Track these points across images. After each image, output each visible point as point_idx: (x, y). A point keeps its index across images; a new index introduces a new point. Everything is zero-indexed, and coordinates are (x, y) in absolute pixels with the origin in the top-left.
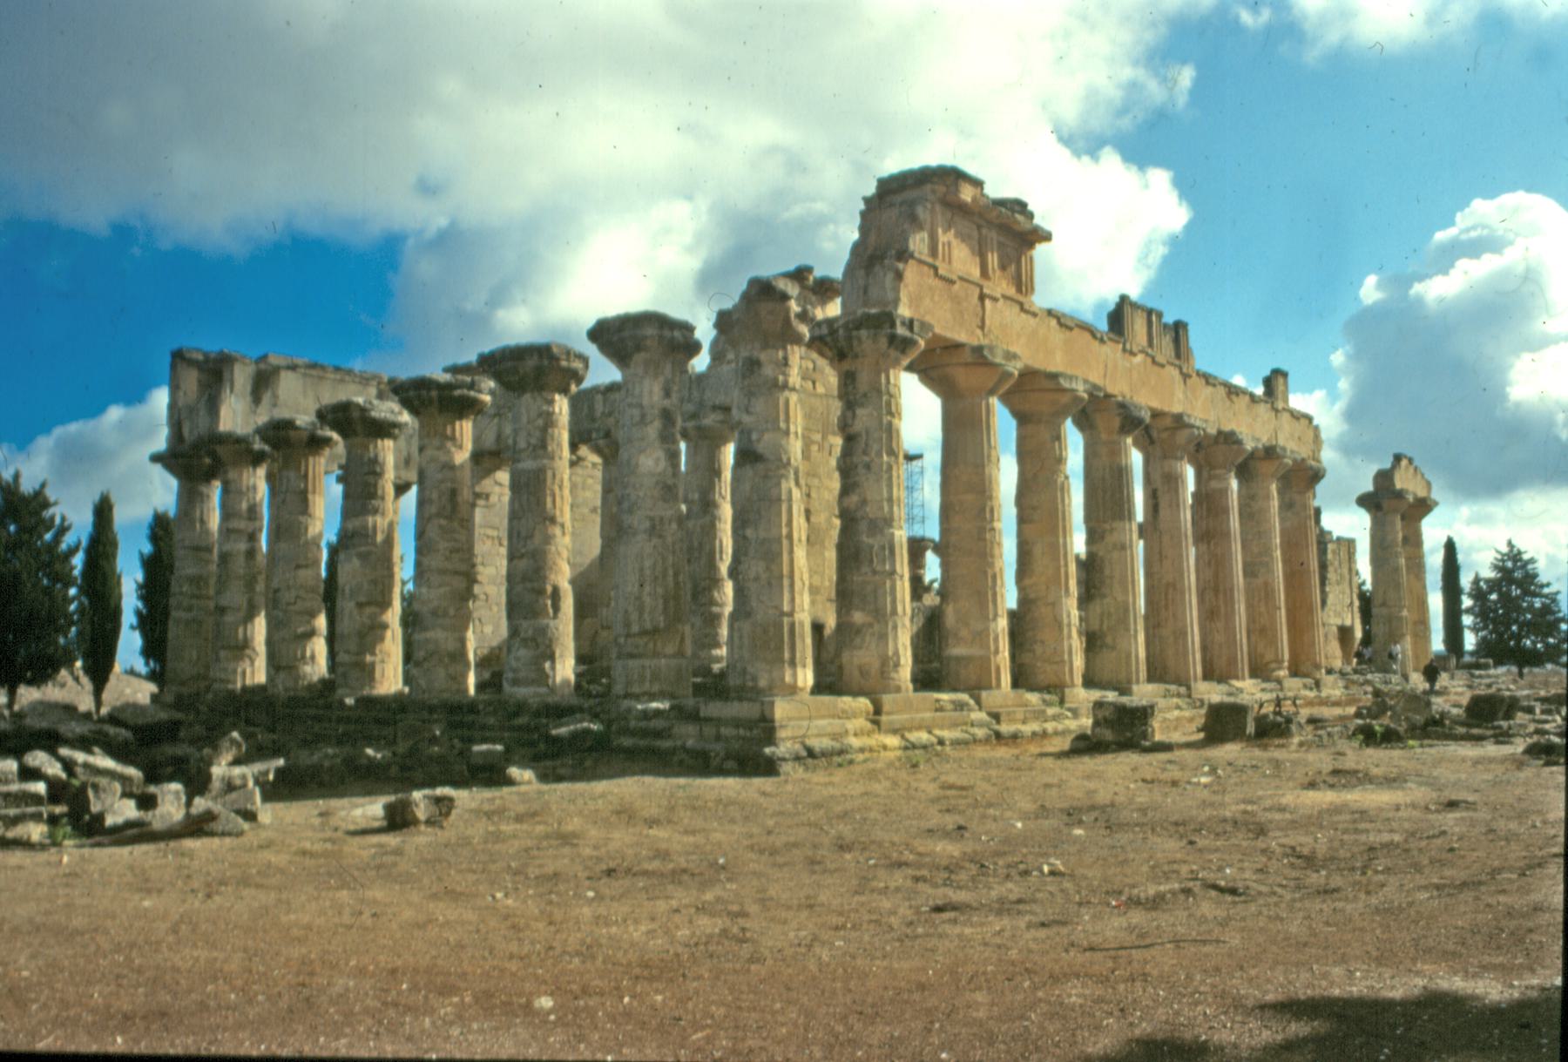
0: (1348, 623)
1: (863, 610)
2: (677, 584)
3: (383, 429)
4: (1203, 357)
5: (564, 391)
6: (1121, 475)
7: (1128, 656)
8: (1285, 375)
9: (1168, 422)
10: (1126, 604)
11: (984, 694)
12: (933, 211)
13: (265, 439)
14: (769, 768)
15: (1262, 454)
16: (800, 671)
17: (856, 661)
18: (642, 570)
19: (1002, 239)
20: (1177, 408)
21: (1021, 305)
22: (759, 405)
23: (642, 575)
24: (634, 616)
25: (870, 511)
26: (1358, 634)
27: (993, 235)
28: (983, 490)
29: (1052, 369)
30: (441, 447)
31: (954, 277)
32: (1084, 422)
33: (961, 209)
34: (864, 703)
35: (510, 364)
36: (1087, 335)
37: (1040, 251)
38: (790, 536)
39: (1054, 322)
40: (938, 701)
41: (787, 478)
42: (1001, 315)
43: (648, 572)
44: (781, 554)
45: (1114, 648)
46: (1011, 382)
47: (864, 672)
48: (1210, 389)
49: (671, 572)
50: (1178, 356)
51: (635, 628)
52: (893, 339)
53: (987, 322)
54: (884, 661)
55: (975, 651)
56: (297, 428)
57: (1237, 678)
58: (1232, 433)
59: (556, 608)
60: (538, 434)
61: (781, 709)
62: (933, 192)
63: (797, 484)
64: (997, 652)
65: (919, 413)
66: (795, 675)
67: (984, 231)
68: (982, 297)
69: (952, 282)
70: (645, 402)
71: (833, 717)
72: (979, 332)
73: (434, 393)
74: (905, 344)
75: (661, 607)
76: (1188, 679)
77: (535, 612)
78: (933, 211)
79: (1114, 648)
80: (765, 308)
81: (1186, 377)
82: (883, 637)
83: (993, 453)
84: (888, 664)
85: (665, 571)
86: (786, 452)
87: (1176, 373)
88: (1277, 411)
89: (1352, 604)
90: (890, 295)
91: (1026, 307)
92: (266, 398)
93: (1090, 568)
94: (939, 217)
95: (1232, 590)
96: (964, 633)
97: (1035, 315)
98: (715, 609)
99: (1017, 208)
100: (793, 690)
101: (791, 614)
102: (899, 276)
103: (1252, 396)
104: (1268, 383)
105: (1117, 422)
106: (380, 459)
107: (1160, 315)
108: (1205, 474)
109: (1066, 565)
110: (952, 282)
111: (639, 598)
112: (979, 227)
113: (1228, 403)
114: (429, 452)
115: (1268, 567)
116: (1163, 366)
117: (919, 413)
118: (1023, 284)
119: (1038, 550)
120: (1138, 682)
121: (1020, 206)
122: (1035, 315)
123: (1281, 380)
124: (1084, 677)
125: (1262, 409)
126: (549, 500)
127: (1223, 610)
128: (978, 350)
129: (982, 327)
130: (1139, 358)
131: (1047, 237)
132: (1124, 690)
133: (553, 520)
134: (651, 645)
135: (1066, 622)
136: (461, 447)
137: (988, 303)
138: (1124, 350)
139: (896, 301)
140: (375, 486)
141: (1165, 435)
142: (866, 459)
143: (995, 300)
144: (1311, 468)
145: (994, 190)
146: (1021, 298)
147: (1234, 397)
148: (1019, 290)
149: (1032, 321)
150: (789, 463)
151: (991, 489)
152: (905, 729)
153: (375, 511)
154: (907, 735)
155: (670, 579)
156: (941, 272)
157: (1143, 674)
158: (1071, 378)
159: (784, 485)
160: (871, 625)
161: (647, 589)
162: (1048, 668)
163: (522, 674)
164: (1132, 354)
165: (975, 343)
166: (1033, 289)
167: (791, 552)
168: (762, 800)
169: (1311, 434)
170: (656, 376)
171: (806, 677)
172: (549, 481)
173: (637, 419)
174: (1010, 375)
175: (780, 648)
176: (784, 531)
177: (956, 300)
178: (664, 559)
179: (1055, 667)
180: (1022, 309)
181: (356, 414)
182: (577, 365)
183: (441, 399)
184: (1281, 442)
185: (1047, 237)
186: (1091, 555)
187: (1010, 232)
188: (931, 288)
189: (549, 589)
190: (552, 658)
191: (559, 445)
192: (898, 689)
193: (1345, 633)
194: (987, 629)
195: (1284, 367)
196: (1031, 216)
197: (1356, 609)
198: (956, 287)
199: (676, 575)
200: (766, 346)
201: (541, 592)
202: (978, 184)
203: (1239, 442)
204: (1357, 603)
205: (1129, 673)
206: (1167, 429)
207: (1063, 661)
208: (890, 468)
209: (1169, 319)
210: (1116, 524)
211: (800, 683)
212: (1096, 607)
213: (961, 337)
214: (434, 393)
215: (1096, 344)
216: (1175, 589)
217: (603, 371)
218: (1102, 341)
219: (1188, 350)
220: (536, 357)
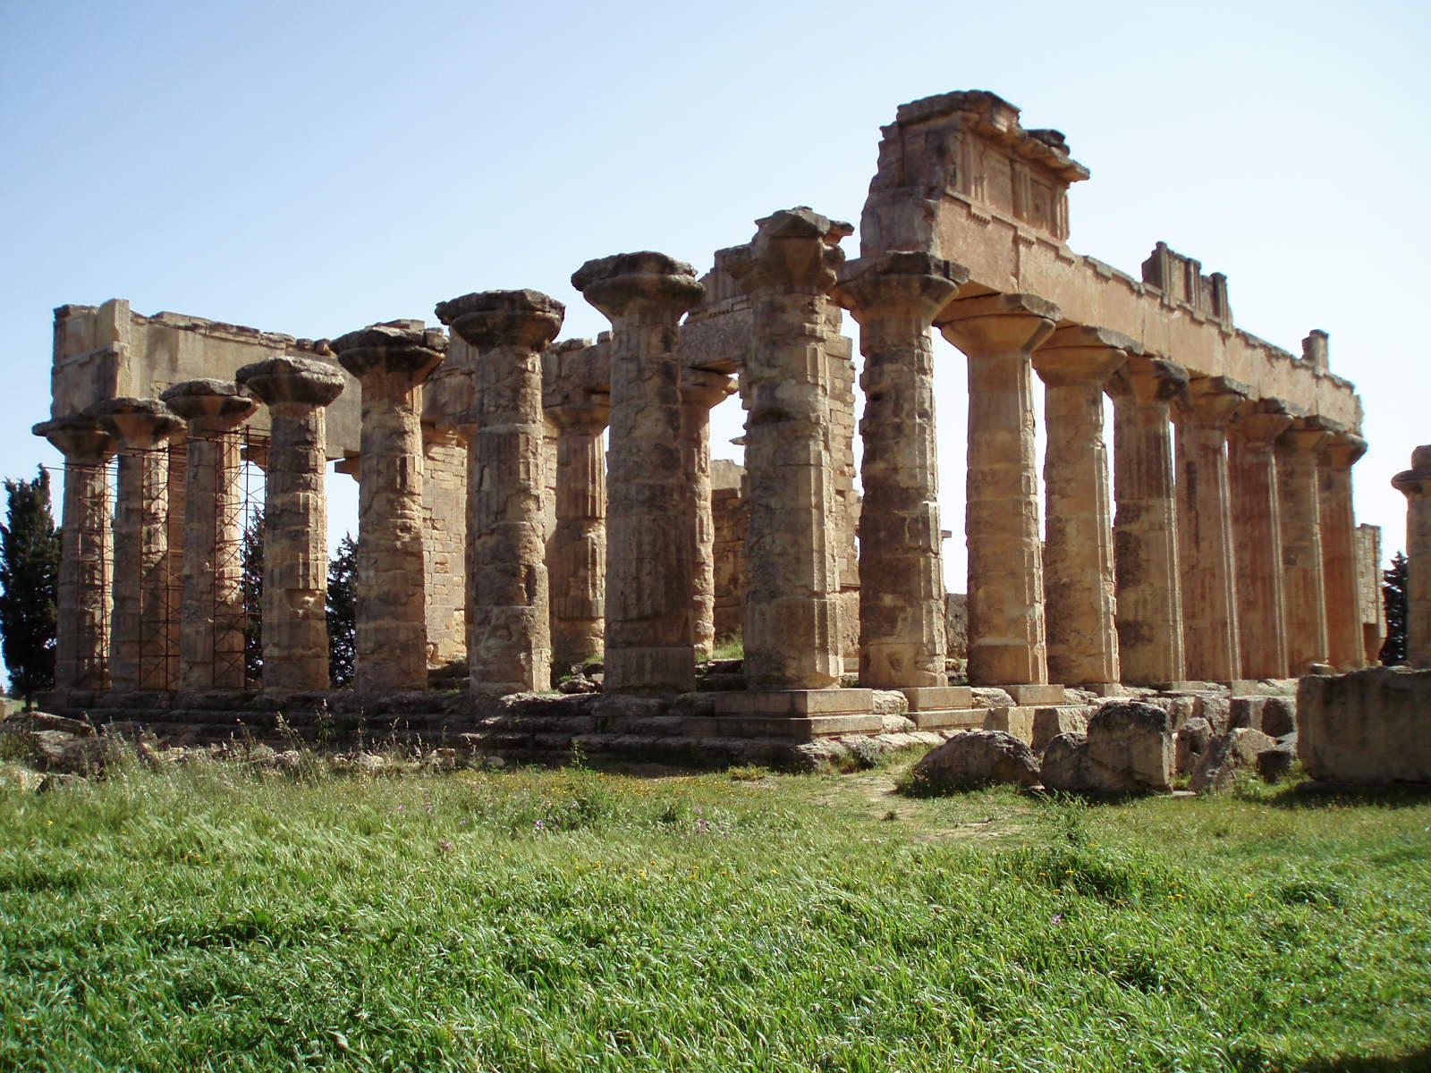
0: (1372, 620)
1: (893, 592)
2: (679, 560)
3: (325, 394)
4: (1245, 312)
5: (538, 348)
6: (1159, 441)
7: (1167, 649)
8: (1325, 336)
9: (1205, 387)
10: (1164, 588)
11: (1022, 689)
12: (963, 143)
13: (172, 407)
14: (804, 765)
15: (1301, 425)
16: (831, 657)
17: (886, 650)
18: (639, 545)
19: (1035, 176)
20: (1215, 372)
21: (1056, 249)
22: (782, 357)
23: (640, 552)
24: (632, 599)
25: (903, 480)
26: (1383, 633)
27: (1026, 171)
28: (1016, 455)
29: (1087, 322)
30: (390, 410)
31: (989, 218)
32: (1119, 388)
33: (993, 139)
34: (894, 696)
35: (475, 314)
36: (1124, 288)
37: (1075, 191)
38: (820, 506)
39: (1089, 272)
40: (975, 695)
41: (816, 440)
42: (1036, 263)
43: (646, 548)
44: (810, 525)
45: (1150, 640)
46: (1048, 335)
47: (894, 662)
48: (1249, 352)
49: (673, 549)
50: (1216, 311)
51: (633, 613)
52: (927, 285)
53: (1022, 270)
54: (918, 647)
55: (1011, 640)
56: (212, 393)
57: (1277, 677)
58: (1273, 401)
59: (532, 593)
60: (508, 393)
61: (815, 702)
62: (965, 120)
63: (827, 448)
64: (1034, 641)
65: (947, 371)
66: (827, 663)
67: (1018, 167)
68: (1017, 240)
69: (985, 222)
70: (643, 354)
71: (867, 712)
72: (1013, 279)
73: (382, 350)
74: (934, 290)
75: (662, 589)
76: (1227, 676)
77: (506, 598)
78: (963, 143)
79: (1150, 640)
80: (793, 246)
81: (1225, 336)
82: (917, 623)
83: (1029, 416)
84: (925, 653)
85: (667, 546)
86: (815, 411)
87: (1214, 331)
88: (1317, 377)
89: (1377, 601)
90: (920, 236)
91: (1062, 253)
92: (162, 356)
94: (971, 148)
95: (1271, 578)
96: (997, 619)
97: (1070, 262)
98: (697, 598)
99: (1053, 141)
100: (826, 680)
101: (821, 595)
102: (930, 214)
103: (1292, 359)
104: (1308, 344)
105: (1154, 385)
106: (312, 426)
107: (1198, 266)
108: (1240, 446)
109: (1104, 546)
110: (985, 222)
111: (637, 578)
112: (1012, 162)
113: (1268, 365)
114: (375, 416)
115: (1308, 552)
116: (1200, 323)
117: (947, 371)
118: (1059, 228)
119: (1071, 529)
120: (1177, 679)
121: (1056, 138)
122: (1070, 262)
123: (1321, 341)
124: (1189, 665)
125: (1304, 375)
126: (522, 468)
127: (1261, 601)
128: (1015, 299)
129: (1016, 275)
130: (1177, 314)
131: (1085, 175)
132: (1162, 689)
133: (526, 491)
134: (651, 632)
135: (1103, 609)
136: (411, 411)
137: (1022, 248)
138: (1162, 305)
139: (928, 243)
140: (307, 457)
141: (1202, 401)
142: (897, 420)
143: (1029, 243)
144: (1353, 442)
145: (1028, 122)
146: (1053, 241)
147: (1274, 360)
148: (1054, 234)
149: (1068, 269)
150: (817, 423)
151: (1027, 458)
152: (943, 727)
153: (307, 486)
154: (946, 733)
155: (673, 557)
156: (974, 210)
157: (1182, 671)
158: (1107, 332)
159: (812, 446)
160: (902, 609)
161: (647, 568)
162: (1086, 661)
163: (492, 667)
164: (1171, 310)
165: (1011, 292)
166: (1068, 233)
167: (821, 523)
169: (1351, 404)
170: (654, 325)
171: (837, 666)
172: (522, 448)
173: (633, 375)
174: (1050, 327)
175: (810, 633)
176: (813, 500)
177: (988, 242)
178: (665, 533)
179: (1091, 659)
180: (1059, 257)
181: (284, 376)
182: (554, 315)
183: (390, 356)
184: (1322, 413)
185: (1085, 175)
187: (1043, 167)
188: (963, 228)
189: (524, 571)
190: (528, 649)
191: (533, 407)
192: (933, 681)
193: (1370, 629)
194: (1023, 616)
195: (1325, 329)
196: (1066, 150)
197: (1381, 606)
198: (990, 227)
199: (679, 551)
200: (789, 291)
201: (515, 574)
202: (1014, 112)
203: (1281, 411)
204: (1382, 599)
205: (1167, 669)
206: (1205, 395)
207: (1101, 653)
208: (923, 430)
209: (1206, 271)
210: (1155, 502)
211: (832, 674)
212: (1131, 596)
213: (996, 286)
214: (382, 350)
215: (1134, 297)
216: (1213, 575)
217: (584, 323)
218: (1139, 294)
219: (1227, 309)
220: (507, 306)
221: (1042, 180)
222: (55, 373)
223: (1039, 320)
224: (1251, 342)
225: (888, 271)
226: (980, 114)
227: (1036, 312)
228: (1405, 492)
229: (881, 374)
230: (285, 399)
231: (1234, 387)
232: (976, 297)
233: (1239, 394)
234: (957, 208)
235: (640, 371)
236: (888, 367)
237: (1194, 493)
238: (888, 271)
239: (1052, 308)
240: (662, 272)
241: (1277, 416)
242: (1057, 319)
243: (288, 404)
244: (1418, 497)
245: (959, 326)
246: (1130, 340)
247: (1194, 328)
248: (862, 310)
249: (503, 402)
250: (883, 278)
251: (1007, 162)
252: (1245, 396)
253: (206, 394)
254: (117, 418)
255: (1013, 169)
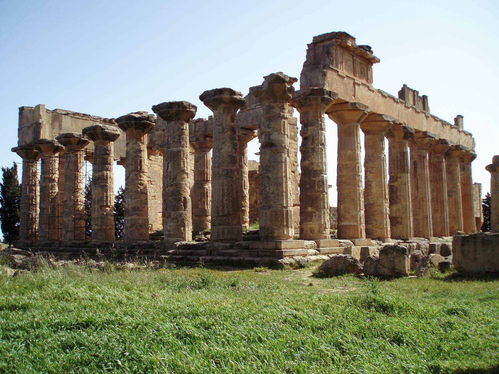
0: (479, 216)
1: (311, 206)
2: (237, 195)
3: (113, 137)
4: (434, 109)
5: (188, 121)
6: (404, 154)
7: (407, 226)
8: (462, 117)
9: (420, 135)
10: (406, 205)
11: (356, 240)
12: (336, 50)
13: (60, 142)
14: (280, 267)
15: (454, 148)
16: (290, 229)
17: (309, 227)
18: (223, 190)
19: (361, 62)
20: (424, 130)
21: (368, 87)
22: (273, 124)
23: (223, 192)
24: (220, 209)
25: (315, 167)
26: (482, 221)
27: (358, 60)
28: (354, 159)
29: (379, 112)
30: (136, 143)
31: (345, 76)
32: (390, 135)
33: (346, 48)
34: (312, 242)
35: (166, 110)
36: (392, 101)
37: (375, 67)
38: (286, 177)
39: (380, 95)
40: (340, 242)
41: (285, 153)
42: (361, 92)
43: (225, 191)
44: (282, 183)
45: (401, 223)
46: (366, 117)
47: (312, 231)
48: (436, 123)
49: (235, 191)
50: (424, 109)
51: (221, 214)
52: (323, 99)
53: (356, 94)
54: (320, 226)
55: (353, 223)
56: (74, 137)
57: (445, 236)
58: (444, 140)
59: (185, 207)
60: (177, 137)
61: (284, 245)
62: (337, 42)
63: (288, 156)
64: (361, 224)
65: (330, 129)
66: (288, 231)
67: (355, 58)
68: (355, 84)
69: (344, 77)
70: (224, 123)
71: (302, 248)
72: (353, 97)
73: (133, 122)
74: (326, 101)
75: (231, 205)
76: (428, 236)
77: (176, 208)
78: (336, 50)
79: (401, 223)
80: (277, 86)
81: (427, 117)
82: (320, 217)
83: (359, 145)
84: (322, 228)
85: (232, 190)
86: (284, 143)
87: (423, 115)
88: (459, 132)
89: (480, 209)
90: (321, 82)
91: (370, 88)
92: (56, 124)
93: (339, 214)
94: (339, 52)
95: (443, 201)
96: (348, 216)
97: (373, 91)
98: (243, 208)
99: (367, 49)
100: (288, 237)
101: (286, 207)
102: (324, 75)
103: (451, 125)
104: (456, 120)
105: (402, 134)
106: (109, 149)
107: (418, 93)
108: (433, 155)
109: (385, 190)
110: (344, 77)
111: (222, 201)
112: (353, 56)
113: (442, 127)
114: (131, 145)
115: (456, 192)
116: (419, 113)
117: (330, 129)
118: (369, 79)
119: (373, 184)
120: (410, 237)
121: (368, 48)
122: (373, 91)
123: (461, 119)
125: (455, 131)
126: (182, 163)
127: (440, 210)
128: (354, 104)
129: (354, 96)
130: (411, 109)
131: (378, 61)
132: (405, 240)
133: (183, 171)
134: (227, 220)
135: (385, 212)
136: (143, 143)
137: (356, 87)
138: (405, 106)
139: (324, 85)
140: (107, 159)
141: (419, 140)
142: (313, 146)
143: (359, 85)
144: (472, 154)
145: (358, 43)
146: (367, 84)
147: (444, 126)
148: (367, 81)
149: (372, 94)
150: (285, 147)
151: (358, 160)
152: (329, 253)
153: (107, 170)
154: (330, 255)
155: (235, 194)
156: (340, 73)
157: (412, 234)
158: (386, 116)
159: (283, 156)
160: (315, 212)
161: (226, 198)
162: (379, 230)
163: (172, 233)
164: (408, 108)
165: (353, 102)
166: (372, 81)
167: (286, 182)
168: (405, 226)
169: (471, 141)
170: (228, 113)
171: (292, 232)
172: (182, 156)
173: (221, 131)
174: (366, 114)
175: (283, 221)
176: (284, 174)
177: (345, 84)
178: (232, 186)
179: (381, 230)
180: (369, 90)
181: (99, 131)
182: (193, 110)
183: (136, 124)
184: (461, 144)
185: (378, 61)
186: (338, 209)
187: (364, 58)
188: (336, 79)
189: (183, 199)
190: (184, 226)
191: (186, 142)
192: (325, 237)
194: (357, 215)
195: (462, 115)
196: (372, 52)
197: (482, 211)
198: (345, 79)
199: (237, 192)
200: (275, 101)
201: (179, 200)
202: (354, 39)
203: (447, 143)
204: (482, 209)
205: (407, 233)
206: (420, 138)
207: (384, 228)
208: (322, 150)
209: (421, 95)
210: (403, 175)
211: (290, 235)
212: (394, 208)
213: (347, 100)
214: (133, 122)
215: (395, 103)
216: (423, 201)
217: (204, 113)
218: (397, 102)
219: (428, 108)
220: (177, 107)
221: (363, 63)
222: (19, 130)
223: (362, 112)
224: (436, 119)
225: (310, 95)
226: (342, 40)
227: (361, 109)
228: (490, 172)
229: (307, 130)
230: (99, 139)
231: (430, 135)
232: (340, 104)
233: (432, 137)
234: (334, 73)
235: (223, 129)
236: (310, 128)
237: (417, 172)
238: (310, 95)
239: (367, 107)
240: (231, 95)
241: (445, 145)
242: (369, 111)
243: (100, 141)
244: (494, 173)
245: (334, 114)
246: (394, 118)
247: (416, 114)
248: (301, 108)
249: (176, 140)
250: (308, 97)
251: (351, 56)
252: (434, 138)
253: (72, 137)
254: (41, 146)
255: (353, 59)
